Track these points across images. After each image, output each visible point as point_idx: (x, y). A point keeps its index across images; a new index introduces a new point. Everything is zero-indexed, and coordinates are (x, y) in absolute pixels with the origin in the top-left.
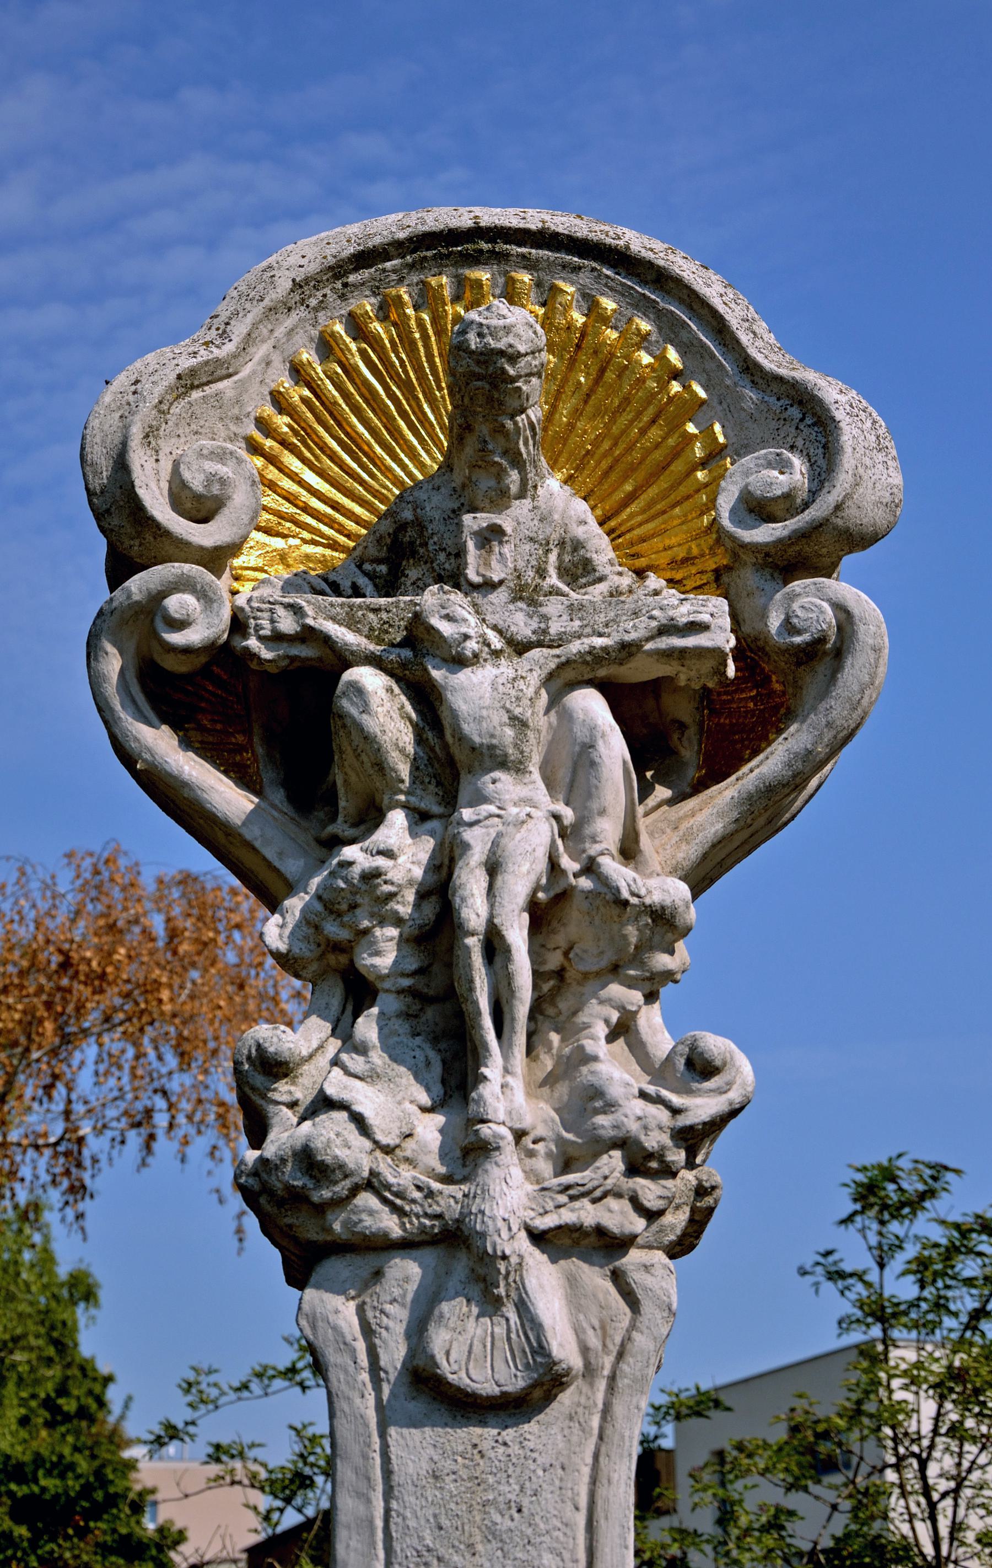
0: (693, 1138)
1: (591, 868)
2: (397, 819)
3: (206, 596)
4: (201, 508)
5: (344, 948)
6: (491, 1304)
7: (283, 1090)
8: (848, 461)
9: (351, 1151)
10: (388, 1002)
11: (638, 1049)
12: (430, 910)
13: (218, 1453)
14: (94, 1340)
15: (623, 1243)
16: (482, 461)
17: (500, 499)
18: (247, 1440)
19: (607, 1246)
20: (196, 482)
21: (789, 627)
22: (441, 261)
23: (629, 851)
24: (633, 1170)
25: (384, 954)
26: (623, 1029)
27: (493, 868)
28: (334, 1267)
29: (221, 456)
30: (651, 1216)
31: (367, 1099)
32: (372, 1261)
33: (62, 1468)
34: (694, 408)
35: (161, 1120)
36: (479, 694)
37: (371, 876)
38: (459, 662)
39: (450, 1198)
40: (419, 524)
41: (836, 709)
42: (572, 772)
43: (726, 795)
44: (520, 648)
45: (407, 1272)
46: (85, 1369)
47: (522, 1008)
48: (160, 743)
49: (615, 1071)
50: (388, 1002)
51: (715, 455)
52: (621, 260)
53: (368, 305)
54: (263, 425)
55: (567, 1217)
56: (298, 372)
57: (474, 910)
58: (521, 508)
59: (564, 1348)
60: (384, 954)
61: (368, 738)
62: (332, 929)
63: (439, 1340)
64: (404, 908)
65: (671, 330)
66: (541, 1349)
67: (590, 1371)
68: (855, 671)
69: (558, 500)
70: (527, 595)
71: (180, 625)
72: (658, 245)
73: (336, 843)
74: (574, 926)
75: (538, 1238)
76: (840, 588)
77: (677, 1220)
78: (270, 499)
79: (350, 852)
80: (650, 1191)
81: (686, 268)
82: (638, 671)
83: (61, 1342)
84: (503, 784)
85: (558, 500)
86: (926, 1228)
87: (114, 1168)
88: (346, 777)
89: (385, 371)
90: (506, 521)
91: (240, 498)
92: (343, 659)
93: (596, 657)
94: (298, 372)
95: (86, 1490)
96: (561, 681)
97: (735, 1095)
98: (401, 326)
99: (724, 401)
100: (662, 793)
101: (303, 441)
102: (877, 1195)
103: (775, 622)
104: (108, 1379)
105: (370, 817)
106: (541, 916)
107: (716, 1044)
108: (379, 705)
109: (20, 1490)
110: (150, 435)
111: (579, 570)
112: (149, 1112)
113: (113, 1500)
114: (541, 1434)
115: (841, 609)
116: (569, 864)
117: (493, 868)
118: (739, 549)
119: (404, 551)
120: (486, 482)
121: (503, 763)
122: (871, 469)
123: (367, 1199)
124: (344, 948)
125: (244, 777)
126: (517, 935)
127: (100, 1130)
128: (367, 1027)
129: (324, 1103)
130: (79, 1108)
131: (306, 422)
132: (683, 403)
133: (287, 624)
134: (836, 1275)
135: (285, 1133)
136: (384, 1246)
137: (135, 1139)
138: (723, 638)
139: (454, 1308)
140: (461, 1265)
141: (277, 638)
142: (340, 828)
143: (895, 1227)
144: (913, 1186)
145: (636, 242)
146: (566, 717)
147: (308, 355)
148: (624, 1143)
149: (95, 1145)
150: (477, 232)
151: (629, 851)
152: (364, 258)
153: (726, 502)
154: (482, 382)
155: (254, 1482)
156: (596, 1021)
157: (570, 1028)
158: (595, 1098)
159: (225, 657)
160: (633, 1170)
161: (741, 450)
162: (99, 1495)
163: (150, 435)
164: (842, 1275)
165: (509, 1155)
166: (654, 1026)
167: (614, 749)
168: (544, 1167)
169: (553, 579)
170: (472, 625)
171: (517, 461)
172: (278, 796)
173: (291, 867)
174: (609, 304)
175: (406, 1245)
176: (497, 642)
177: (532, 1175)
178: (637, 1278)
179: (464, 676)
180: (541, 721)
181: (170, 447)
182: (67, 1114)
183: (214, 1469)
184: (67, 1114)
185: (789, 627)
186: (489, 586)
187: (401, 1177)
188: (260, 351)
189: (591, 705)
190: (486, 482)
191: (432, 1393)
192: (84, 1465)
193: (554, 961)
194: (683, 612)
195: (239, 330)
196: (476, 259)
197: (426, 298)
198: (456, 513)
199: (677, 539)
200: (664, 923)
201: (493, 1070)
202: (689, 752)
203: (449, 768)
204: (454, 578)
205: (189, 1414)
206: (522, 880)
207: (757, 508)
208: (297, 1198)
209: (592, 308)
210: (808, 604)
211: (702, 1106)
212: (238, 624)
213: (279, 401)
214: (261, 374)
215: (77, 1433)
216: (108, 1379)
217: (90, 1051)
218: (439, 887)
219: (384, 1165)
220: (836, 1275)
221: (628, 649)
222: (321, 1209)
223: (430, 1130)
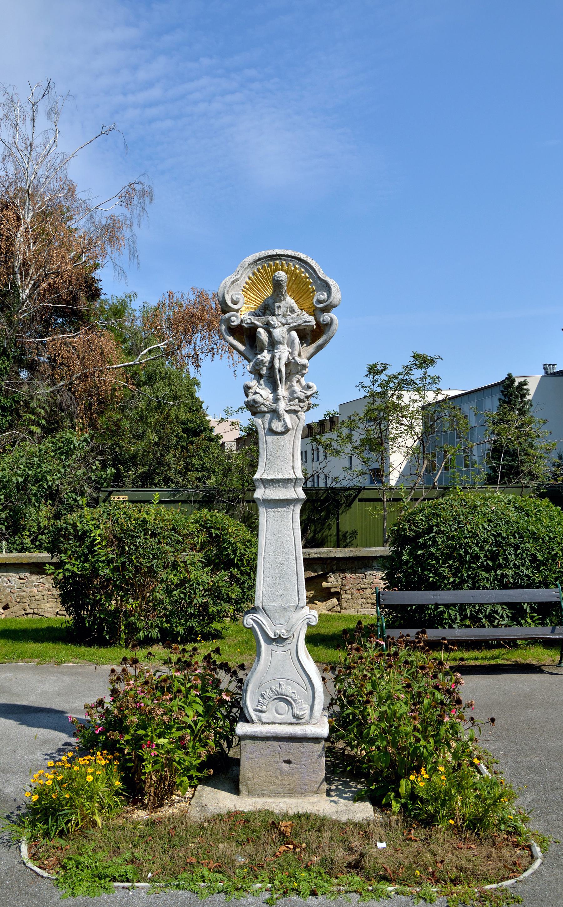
0: (307, 397)
1: (294, 358)
2: (266, 351)
3: (237, 317)
4: (235, 303)
5: (259, 370)
6: (280, 420)
7: (250, 391)
8: (333, 295)
9: (260, 400)
10: (265, 378)
11: (300, 384)
12: (271, 365)
13: (233, 423)
14: (199, 394)
15: (298, 412)
16: (278, 295)
17: (280, 301)
18: (239, 421)
19: (295, 412)
20: (235, 299)
21: (323, 321)
22: (271, 260)
23: (299, 355)
24: (299, 402)
25: (264, 371)
26: (298, 381)
27: (280, 359)
28: (258, 415)
29: (238, 294)
30: (302, 408)
31: (262, 392)
32: (262, 415)
33: (193, 422)
34: (310, 283)
35: (215, 350)
36: (278, 333)
37: (262, 360)
38: (274, 328)
39: (274, 406)
40: (268, 305)
41: (330, 333)
42: (291, 344)
43: (314, 346)
44: (284, 325)
45: (268, 416)
46: (197, 399)
47: (284, 380)
48: (231, 339)
49: (297, 388)
50: (265, 378)
51: (314, 291)
52: (299, 259)
53: (260, 267)
54: (244, 287)
55: (290, 408)
56: (250, 278)
57: (277, 366)
58: (284, 302)
59: (290, 426)
60: (264, 371)
61: (261, 340)
62: (257, 368)
63: (273, 425)
64: (267, 365)
65: (307, 271)
66: (286, 426)
67: (293, 428)
68: (333, 327)
69: (289, 300)
70: (285, 316)
71: (233, 322)
72: (305, 256)
73: (257, 354)
74: (291, 366)
75: (286, 411)
76: (331, 314)
77: (305, 408)
78: (246, 299)
79: (259, 356)
80: (302, 404)
81: (309, 260)
82: (301, 328)
83: (192, 395)
84: (281, 346)
85: (289, 300)
86: (383, 377)
87: (206, 362)
88: (258, 344)
89: (263, 277)
90: (281, 305)
91: (241, 301)
92: (257, 327)
93: (294, 326)
94: (250, 278)
95: (199, 427)
96: (289, 330)
97: (314, 391)
98: (265, 270)
99: (315, 283)
100: (305, 345)
101: (251, 289)
102: (373, 370)
103: (321, 320)
104: (203, 402)
105: (262, 351)
106: (287, 365)
107: (311, 384)
108: (263, 334)
109: (184, 427)
110: (228, 292)
111: (293, 311)
112: (213, 348)
113: (205, 429)
114: (286, 437)
115: (331, 318)
116: (291, 358)
117: (280, 359)
118: (316, 308)
119: (266, 309)
120: (278, 299)
121: (281, 344)
122: (336, 295)
123: (262, 406)
124: (259, 370)
125: (243, 344)
126: (283, 369)
127: (202, 353)
128: (262, 382)
129: (256, 393)
130: (197, 348)
131: (251, 286)
132: (307, 283)
133: (249, 321)
134: (364, 387)
135: (251, 397)
136: (265, 412)
137: (210, 354)
138: (313, 323)
139: (275, 421)
140: (276, 415)
141: (248, 323)
142: (257, 352)
143: (377, 377)
144: (380, 368)
145: (302, 256)
146: (290, 335)
147: (251, 275)
148: (298, 398)
149: (201, 356)
150: (277, 255)
151: (299, 355)
152: (259, 260)
153: (315, 300)
154: (277, 285)
155: (240, 429)
156: (295, 380)
157: (291, 381)
158: (294, 392)
159: (240, 326)
160: (299, 402)
161: (318, 291)
162: (202, 428)
163: (228, 292)
164: (365, 387)
165: (282, 400)
166: (303, 381)
167: (297, 340)
168: (287, 401)
169: (289, 313)
170: (276, 322)
171: (283, 295)
172: (248, 346)
173: (250, 358)
174: (297, 266)
175: (268, 412)
176: (280, 324)
177: (285, 403)
178: (300, 416)
179: (275, 330)
180: (286, 336)
181: (231, 293)
182: (194, 349)
183: (232, 427)
184: (194, 349)
185: (323, 321)
186: (279, 315)
187: (267, 403)
188: (244, 276)
189: (294, 334)
190: (278, 299)
191: (271, 432)
192: (198, 421)
193: (289, 371)
194: (307, 319)
195: (240, 273)
196: (277, 259)
197: (269, 266)
198: (274, 303)
199: (307, 305)
200: (304, 367)
201: (280, 388)
202: (309, 338)
203: (273, 344)
204: (273, 314)
205: (226, 416)
206: (284, 361)
207: (319, 302)
208: (253, 406)
209: (295, 267)
210: (326, 317)
211: (309, 393)
212: (242, 321)
213: (247, 283)
214: (244, 279)
215: (196, 414)
216: (203, 402)
217: (199, 335)
218: (272, 361)
219: (265, 401)
220: (364, 387)
221: (299, 325)
222: (256, 407)
223: (271, 396)
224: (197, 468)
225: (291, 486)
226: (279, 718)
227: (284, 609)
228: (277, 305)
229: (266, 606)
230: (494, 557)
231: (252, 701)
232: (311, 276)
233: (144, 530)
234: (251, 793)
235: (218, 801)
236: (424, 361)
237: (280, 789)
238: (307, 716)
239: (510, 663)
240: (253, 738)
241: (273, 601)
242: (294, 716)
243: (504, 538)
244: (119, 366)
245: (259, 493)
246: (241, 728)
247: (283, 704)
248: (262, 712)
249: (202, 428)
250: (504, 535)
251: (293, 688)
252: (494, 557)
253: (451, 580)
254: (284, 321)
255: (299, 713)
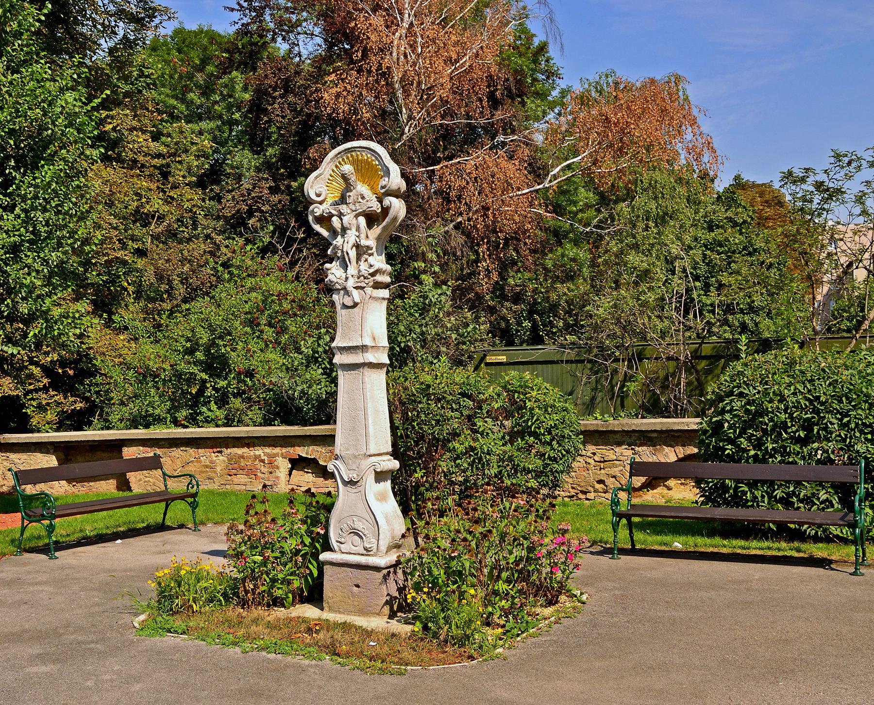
19: (362, 288)
45: (342, 292)
56: (333, 171)
80: (366, 281)
152: (339, 153)
162: (751, 249)
187: (339, 281)
224: (741, 309)
225: (359, 351)
226: (354, 549)
227: (355, 457)
228: (348, 194)
229: (343, 454)
230: (807, 426)
231: (335, 533)
232: (380, 164)
233: (427, 395)
234: (331, 610)
235: (310, 612)
236: (807, 170)
237: (352, 609)
238: (375, 550)
239: (801, 555)
240: (332, 564)
241: (348, 450)
242: (366, 549)
243: (822, 404)
244: (524, 192)
245: (338, 359)
246: (324, 556)
247: (356, 537)
248: (341, 543)
249: (751, 249)
250: (823, 399)
251: (363, 524)
252: (807, 426)
253: (752, 453)
254: (354, 208)
255: (368, 546)
